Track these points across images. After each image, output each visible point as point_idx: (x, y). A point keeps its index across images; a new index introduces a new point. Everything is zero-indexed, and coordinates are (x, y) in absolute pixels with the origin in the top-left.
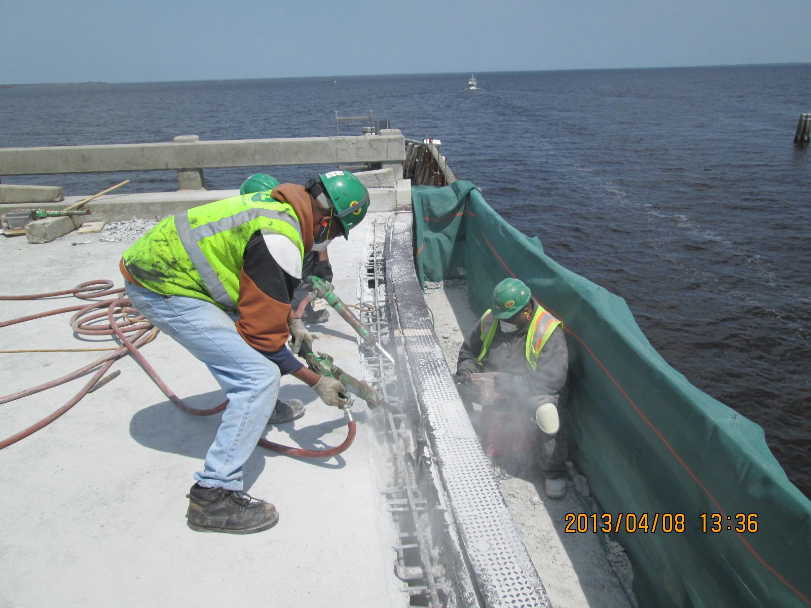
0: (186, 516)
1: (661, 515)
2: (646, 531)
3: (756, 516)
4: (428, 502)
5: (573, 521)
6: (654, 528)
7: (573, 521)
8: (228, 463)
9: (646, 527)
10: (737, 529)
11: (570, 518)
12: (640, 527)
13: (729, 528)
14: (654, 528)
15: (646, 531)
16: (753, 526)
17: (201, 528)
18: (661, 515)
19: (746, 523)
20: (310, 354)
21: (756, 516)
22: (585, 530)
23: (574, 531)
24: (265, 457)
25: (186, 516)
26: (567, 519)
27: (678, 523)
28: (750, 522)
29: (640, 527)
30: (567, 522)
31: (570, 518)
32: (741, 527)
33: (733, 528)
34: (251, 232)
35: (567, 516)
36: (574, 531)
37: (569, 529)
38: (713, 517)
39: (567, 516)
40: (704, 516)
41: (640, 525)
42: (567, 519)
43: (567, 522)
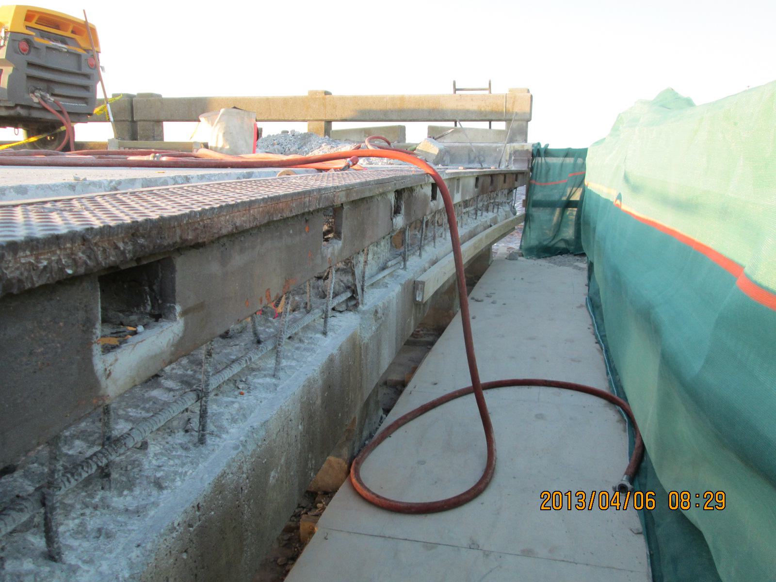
0: (109, 140)
2: (618, 508)
3: (654, 494)
4: (91, 503)
5: (548, 499)
7: (548, 499)
8: (163, 327)
11: (709, 496)
12: (612, 504)
15: (618, 508)
16: (650, 503)
19: (680, 500)
20: (75, 457)
21: (654, 494)
22: (560, 507)
23: (549, 508)
24: (525, 185)
25: (109, 140)
26: (705, 497)
27: (687, 500)
28: (647, 500)
29: (612, 504)
30: (706, 500)
31: (709, 496)
32: (720, 505)
35: (706, 494)
37: (544, 507)
39: (706, 494)
41: (612, 502)
42: (705, 497)
43: (706, 500)
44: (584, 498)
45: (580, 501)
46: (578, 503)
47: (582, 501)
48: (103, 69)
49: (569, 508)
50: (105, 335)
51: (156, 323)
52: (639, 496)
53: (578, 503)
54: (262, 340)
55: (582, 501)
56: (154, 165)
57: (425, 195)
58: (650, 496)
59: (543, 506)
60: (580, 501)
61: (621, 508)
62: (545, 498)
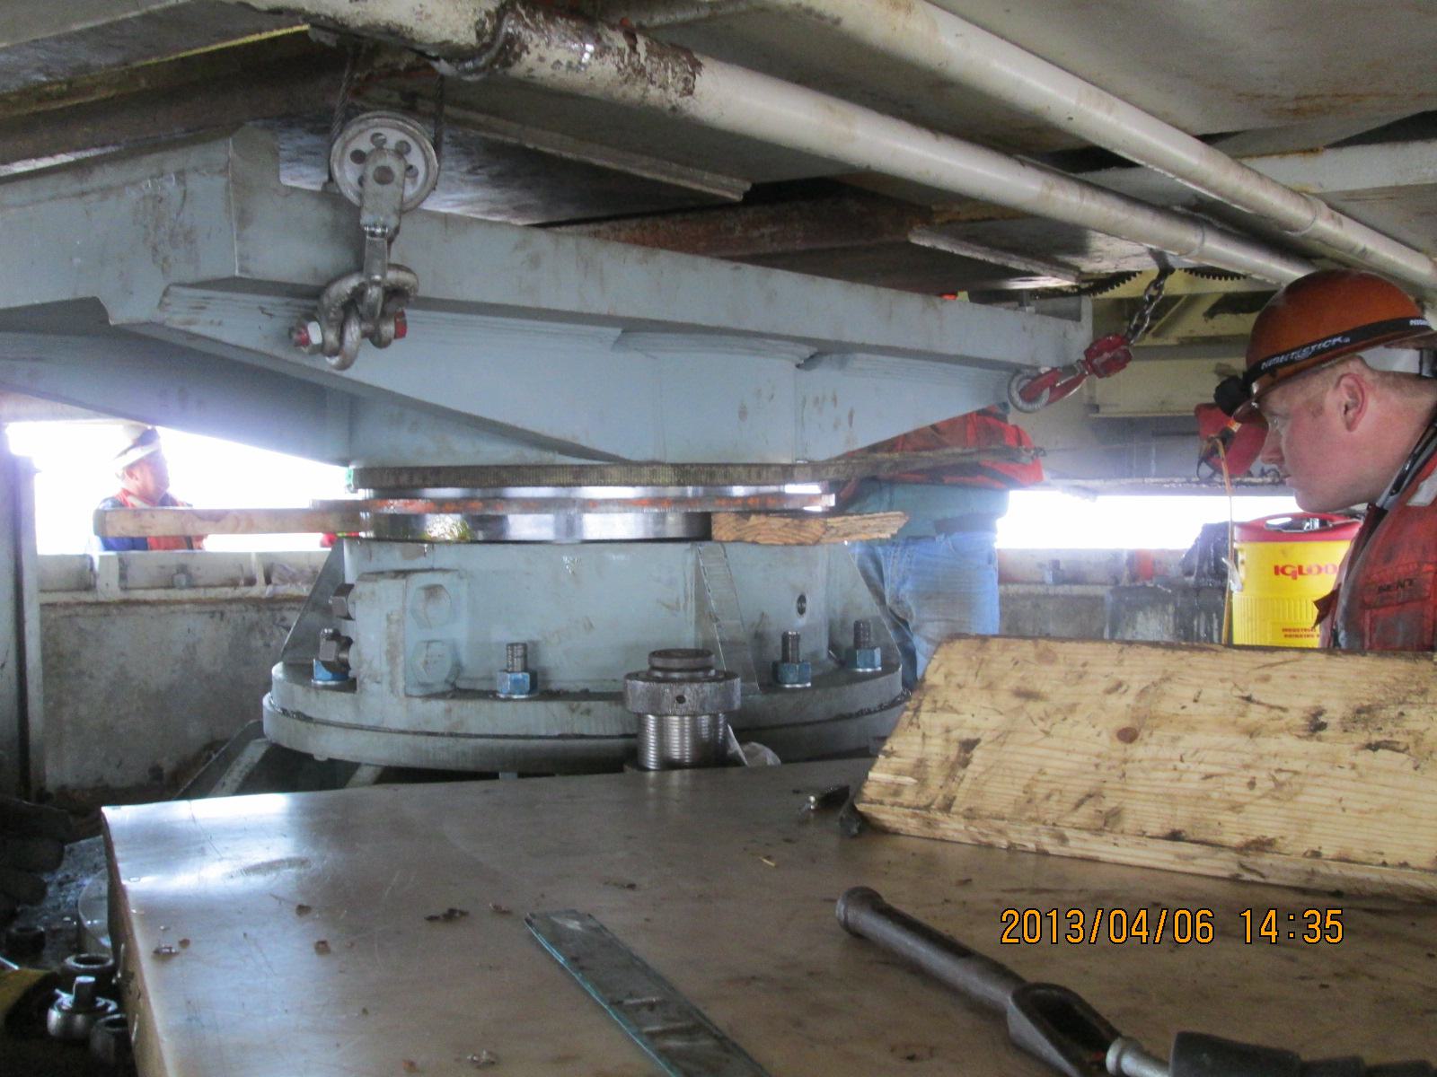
0: (313, 501)
1: (1106, 912)
2: (1144, 941)
3: (1210, 915)
6: (1094, 935)
9: (1144, 933)
10: (1306, 937)
11: (1011, 918)
12: (1134, 933)
13: (1291, 935)
14: (1094, 935)
15: (1144, 941)
17: (616, 508)
18: (1171, 912)
22: (1037, 939)
23: (1017, 941)
26: (1004, 919)
28: (1199, 925)
29: (1134, 933)
30: (1005, 925)
31: (1011, 918)
32: (1075, 934)
33: (1298, 935)
34: (852, 626)
35: (1005, 915)
36: (1017, 941)
38: (1306, 916)
39: (1005, 915)
40: (1248, 914)
41: (1133, 929)
42: (1004, 919)
43: (1005, 925)
44: (1081, 921)
45: (1073, 926)
46: (1071, 932)
47: (1078, 926)
48: (737, 268)
49: (1054, 941)
50: (388, 652)
51: (154, 949)
52: (1183, 918)
53: (1071, 932)
54: (700, 636)
55: (1078, 926)
56: (755, 342)
57: (643, 687)
58: (1204, 917)
59: (1005, 936)
60: (1073, 926)
61: (1151, 941)
62: (1009, 922)
